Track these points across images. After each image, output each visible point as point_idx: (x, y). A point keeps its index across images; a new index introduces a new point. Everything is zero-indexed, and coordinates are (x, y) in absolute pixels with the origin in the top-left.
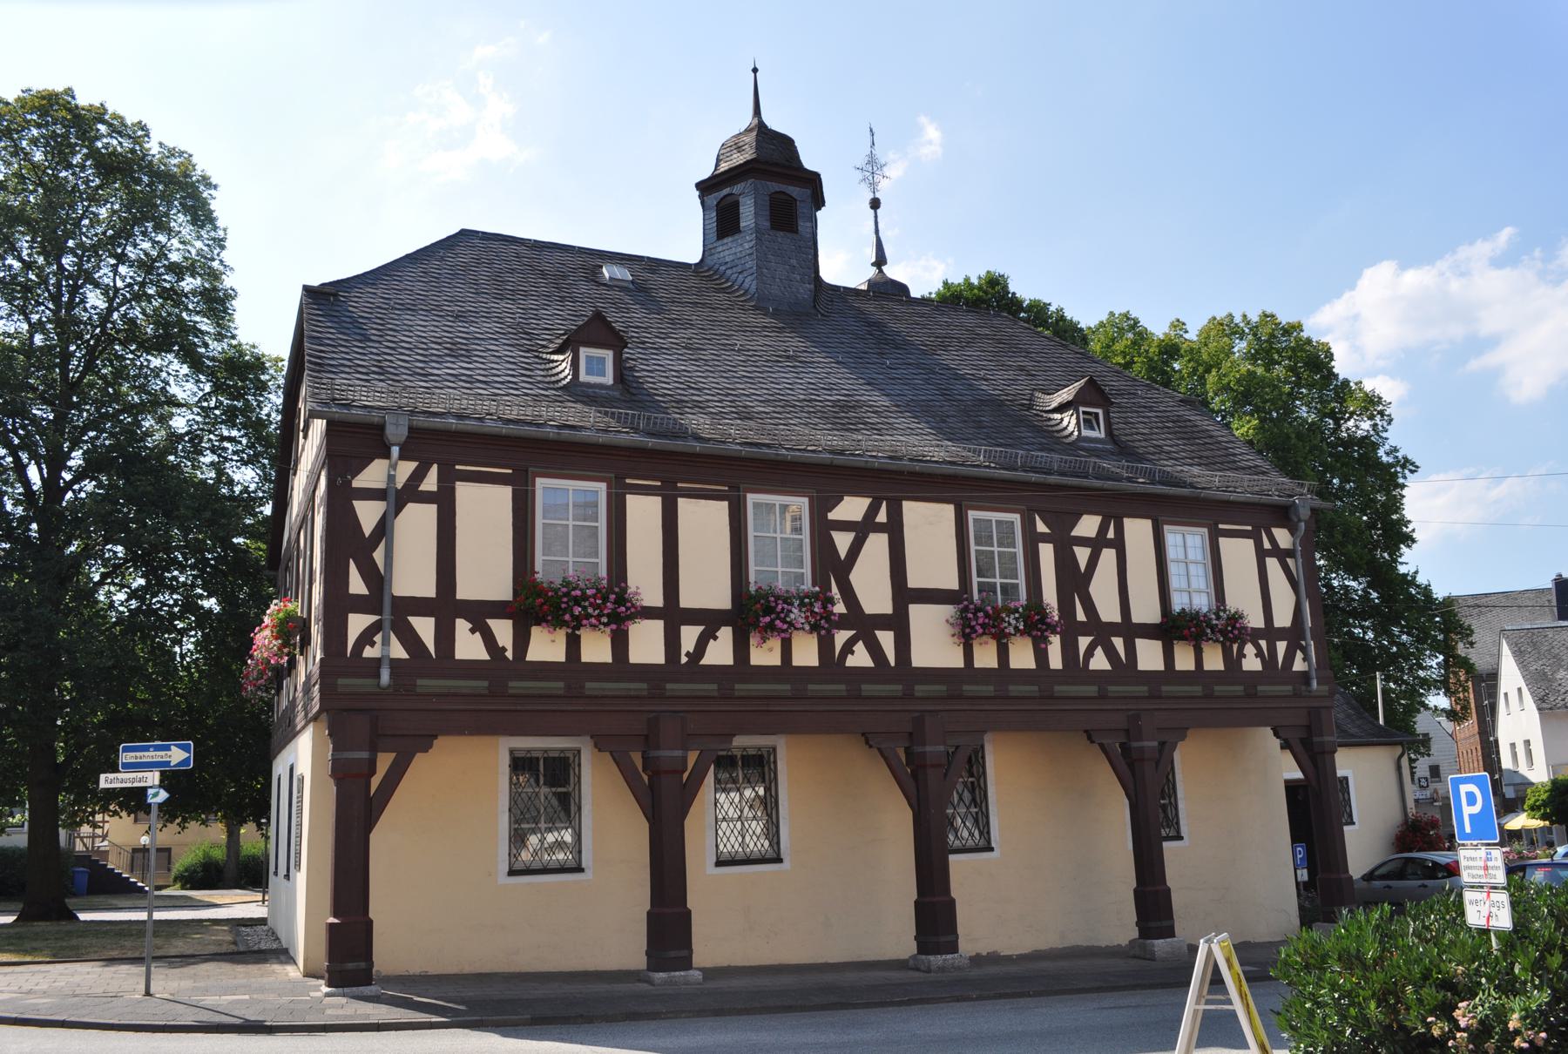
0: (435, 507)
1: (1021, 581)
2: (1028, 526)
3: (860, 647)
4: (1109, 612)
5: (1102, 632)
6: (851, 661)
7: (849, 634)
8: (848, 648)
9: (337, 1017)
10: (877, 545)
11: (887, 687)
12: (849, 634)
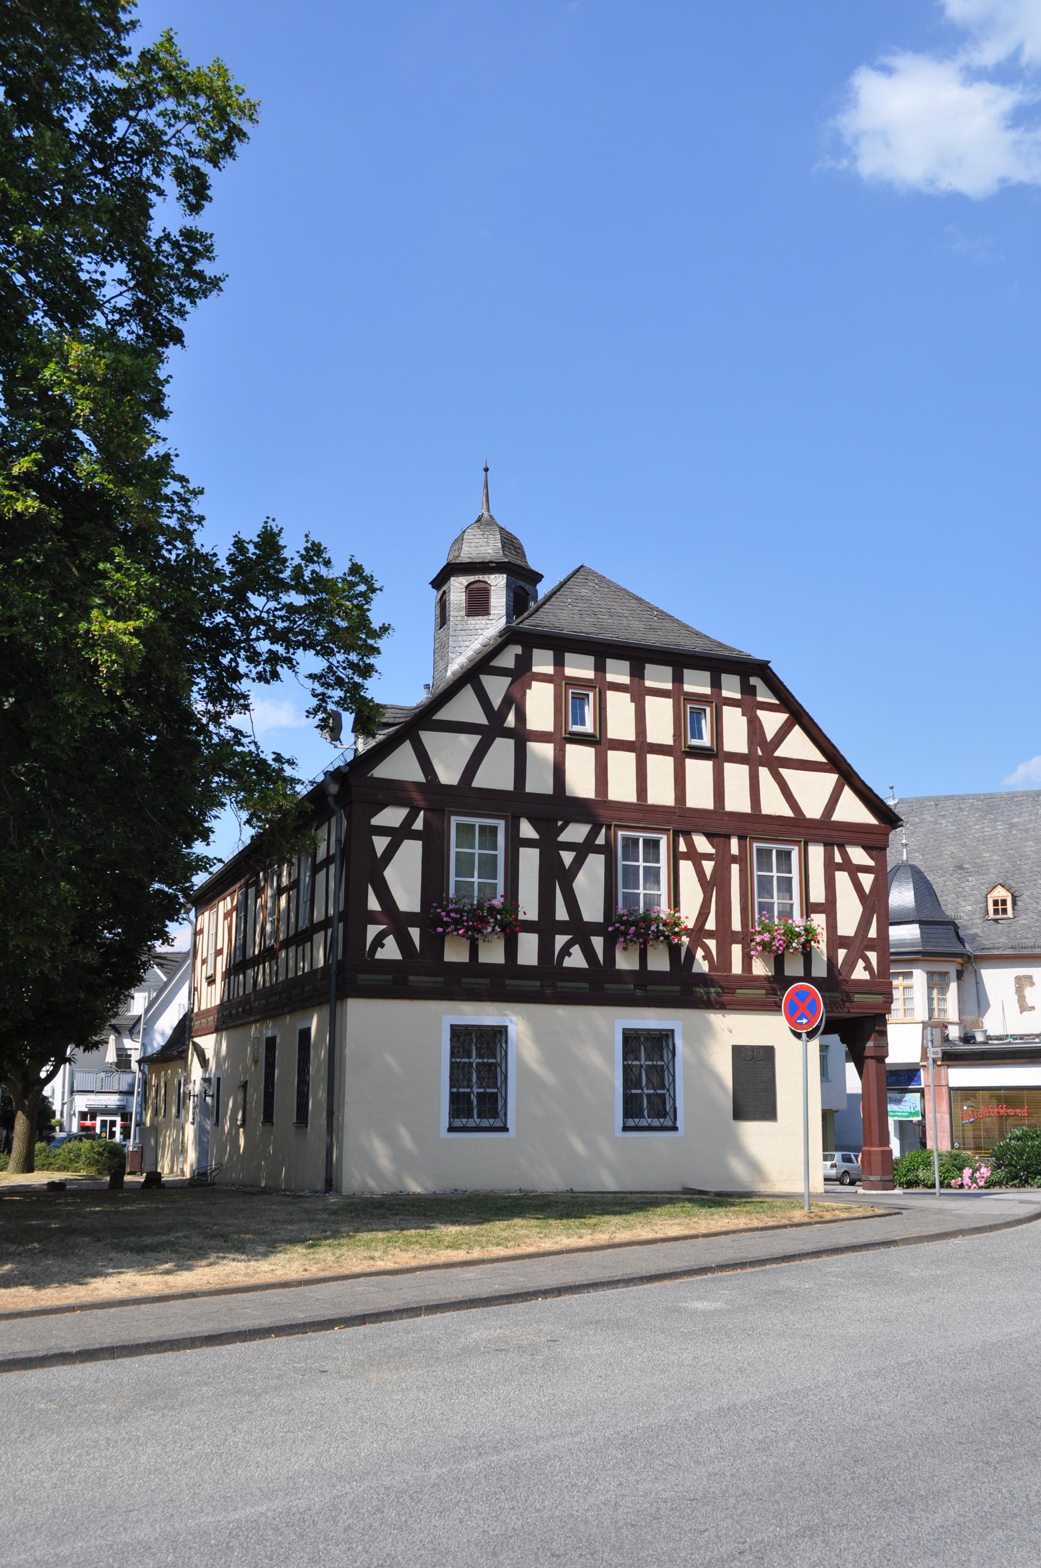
0: (420, 843)
1: (500, 881)
2: (513, 830)
3: (576, 950)
4: (592, 911)
5: (580, 930)
6: (568, 962)
7: (567, 938)
8: (566, 951)
9: (468, 1272)
10: (595, 863)
11: (570, 984)
12: (567, 938)
